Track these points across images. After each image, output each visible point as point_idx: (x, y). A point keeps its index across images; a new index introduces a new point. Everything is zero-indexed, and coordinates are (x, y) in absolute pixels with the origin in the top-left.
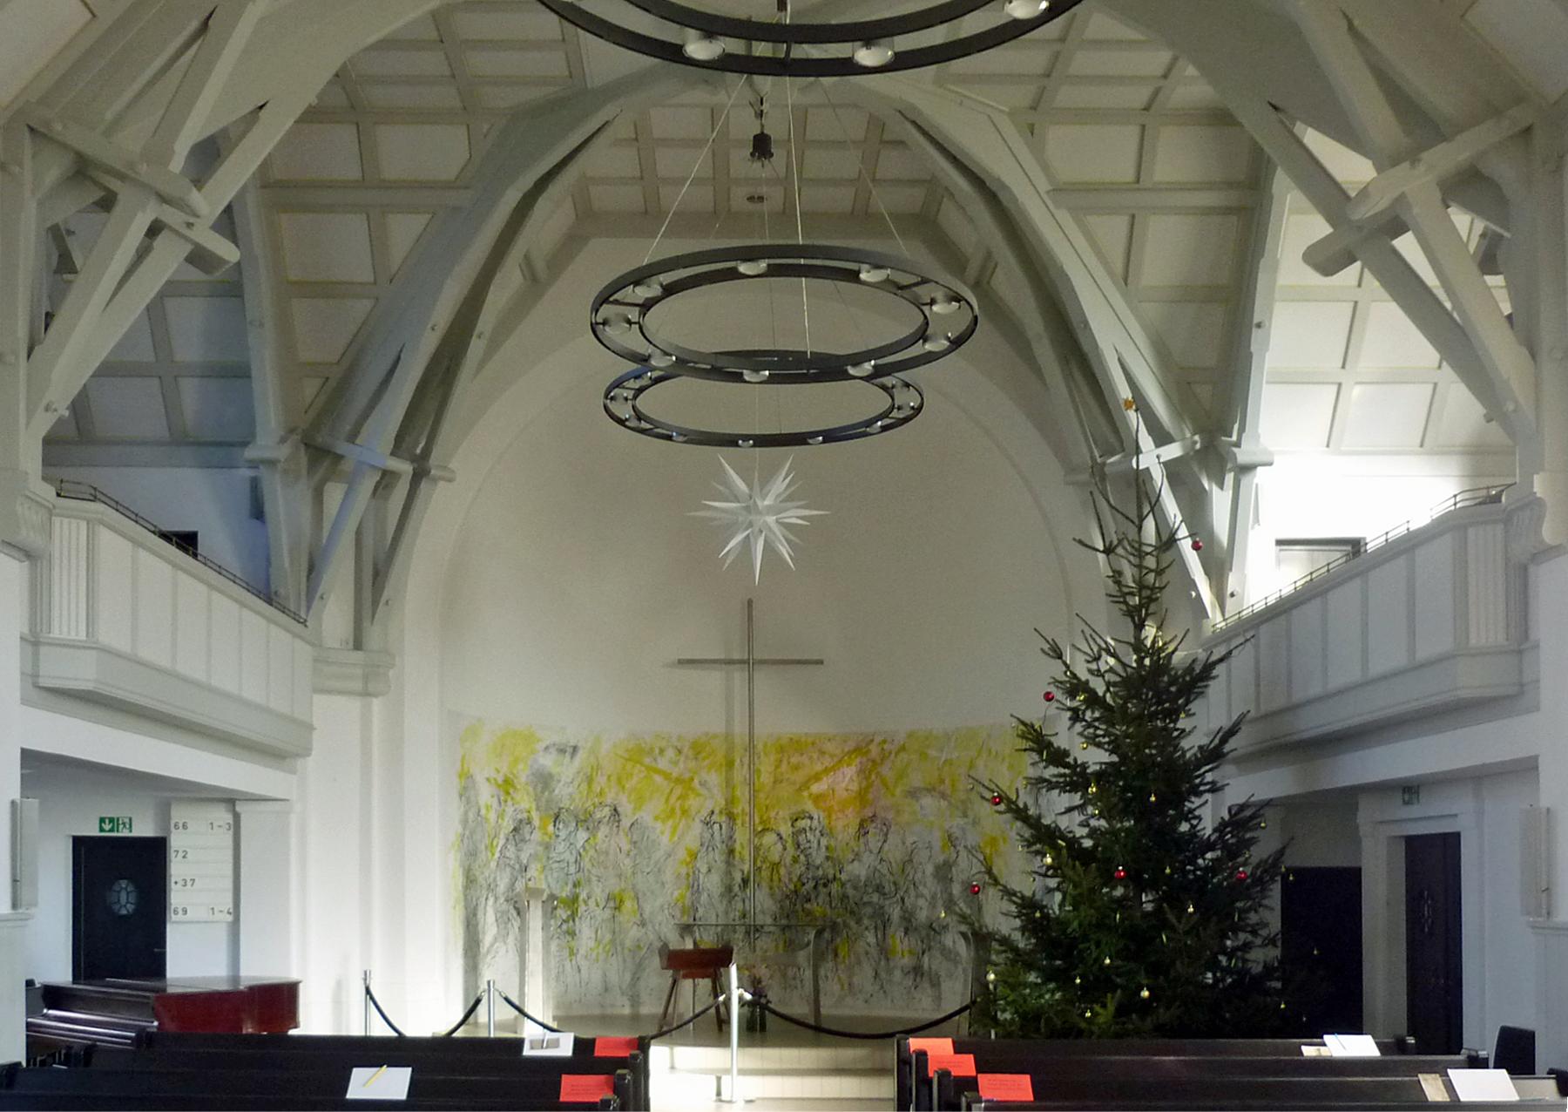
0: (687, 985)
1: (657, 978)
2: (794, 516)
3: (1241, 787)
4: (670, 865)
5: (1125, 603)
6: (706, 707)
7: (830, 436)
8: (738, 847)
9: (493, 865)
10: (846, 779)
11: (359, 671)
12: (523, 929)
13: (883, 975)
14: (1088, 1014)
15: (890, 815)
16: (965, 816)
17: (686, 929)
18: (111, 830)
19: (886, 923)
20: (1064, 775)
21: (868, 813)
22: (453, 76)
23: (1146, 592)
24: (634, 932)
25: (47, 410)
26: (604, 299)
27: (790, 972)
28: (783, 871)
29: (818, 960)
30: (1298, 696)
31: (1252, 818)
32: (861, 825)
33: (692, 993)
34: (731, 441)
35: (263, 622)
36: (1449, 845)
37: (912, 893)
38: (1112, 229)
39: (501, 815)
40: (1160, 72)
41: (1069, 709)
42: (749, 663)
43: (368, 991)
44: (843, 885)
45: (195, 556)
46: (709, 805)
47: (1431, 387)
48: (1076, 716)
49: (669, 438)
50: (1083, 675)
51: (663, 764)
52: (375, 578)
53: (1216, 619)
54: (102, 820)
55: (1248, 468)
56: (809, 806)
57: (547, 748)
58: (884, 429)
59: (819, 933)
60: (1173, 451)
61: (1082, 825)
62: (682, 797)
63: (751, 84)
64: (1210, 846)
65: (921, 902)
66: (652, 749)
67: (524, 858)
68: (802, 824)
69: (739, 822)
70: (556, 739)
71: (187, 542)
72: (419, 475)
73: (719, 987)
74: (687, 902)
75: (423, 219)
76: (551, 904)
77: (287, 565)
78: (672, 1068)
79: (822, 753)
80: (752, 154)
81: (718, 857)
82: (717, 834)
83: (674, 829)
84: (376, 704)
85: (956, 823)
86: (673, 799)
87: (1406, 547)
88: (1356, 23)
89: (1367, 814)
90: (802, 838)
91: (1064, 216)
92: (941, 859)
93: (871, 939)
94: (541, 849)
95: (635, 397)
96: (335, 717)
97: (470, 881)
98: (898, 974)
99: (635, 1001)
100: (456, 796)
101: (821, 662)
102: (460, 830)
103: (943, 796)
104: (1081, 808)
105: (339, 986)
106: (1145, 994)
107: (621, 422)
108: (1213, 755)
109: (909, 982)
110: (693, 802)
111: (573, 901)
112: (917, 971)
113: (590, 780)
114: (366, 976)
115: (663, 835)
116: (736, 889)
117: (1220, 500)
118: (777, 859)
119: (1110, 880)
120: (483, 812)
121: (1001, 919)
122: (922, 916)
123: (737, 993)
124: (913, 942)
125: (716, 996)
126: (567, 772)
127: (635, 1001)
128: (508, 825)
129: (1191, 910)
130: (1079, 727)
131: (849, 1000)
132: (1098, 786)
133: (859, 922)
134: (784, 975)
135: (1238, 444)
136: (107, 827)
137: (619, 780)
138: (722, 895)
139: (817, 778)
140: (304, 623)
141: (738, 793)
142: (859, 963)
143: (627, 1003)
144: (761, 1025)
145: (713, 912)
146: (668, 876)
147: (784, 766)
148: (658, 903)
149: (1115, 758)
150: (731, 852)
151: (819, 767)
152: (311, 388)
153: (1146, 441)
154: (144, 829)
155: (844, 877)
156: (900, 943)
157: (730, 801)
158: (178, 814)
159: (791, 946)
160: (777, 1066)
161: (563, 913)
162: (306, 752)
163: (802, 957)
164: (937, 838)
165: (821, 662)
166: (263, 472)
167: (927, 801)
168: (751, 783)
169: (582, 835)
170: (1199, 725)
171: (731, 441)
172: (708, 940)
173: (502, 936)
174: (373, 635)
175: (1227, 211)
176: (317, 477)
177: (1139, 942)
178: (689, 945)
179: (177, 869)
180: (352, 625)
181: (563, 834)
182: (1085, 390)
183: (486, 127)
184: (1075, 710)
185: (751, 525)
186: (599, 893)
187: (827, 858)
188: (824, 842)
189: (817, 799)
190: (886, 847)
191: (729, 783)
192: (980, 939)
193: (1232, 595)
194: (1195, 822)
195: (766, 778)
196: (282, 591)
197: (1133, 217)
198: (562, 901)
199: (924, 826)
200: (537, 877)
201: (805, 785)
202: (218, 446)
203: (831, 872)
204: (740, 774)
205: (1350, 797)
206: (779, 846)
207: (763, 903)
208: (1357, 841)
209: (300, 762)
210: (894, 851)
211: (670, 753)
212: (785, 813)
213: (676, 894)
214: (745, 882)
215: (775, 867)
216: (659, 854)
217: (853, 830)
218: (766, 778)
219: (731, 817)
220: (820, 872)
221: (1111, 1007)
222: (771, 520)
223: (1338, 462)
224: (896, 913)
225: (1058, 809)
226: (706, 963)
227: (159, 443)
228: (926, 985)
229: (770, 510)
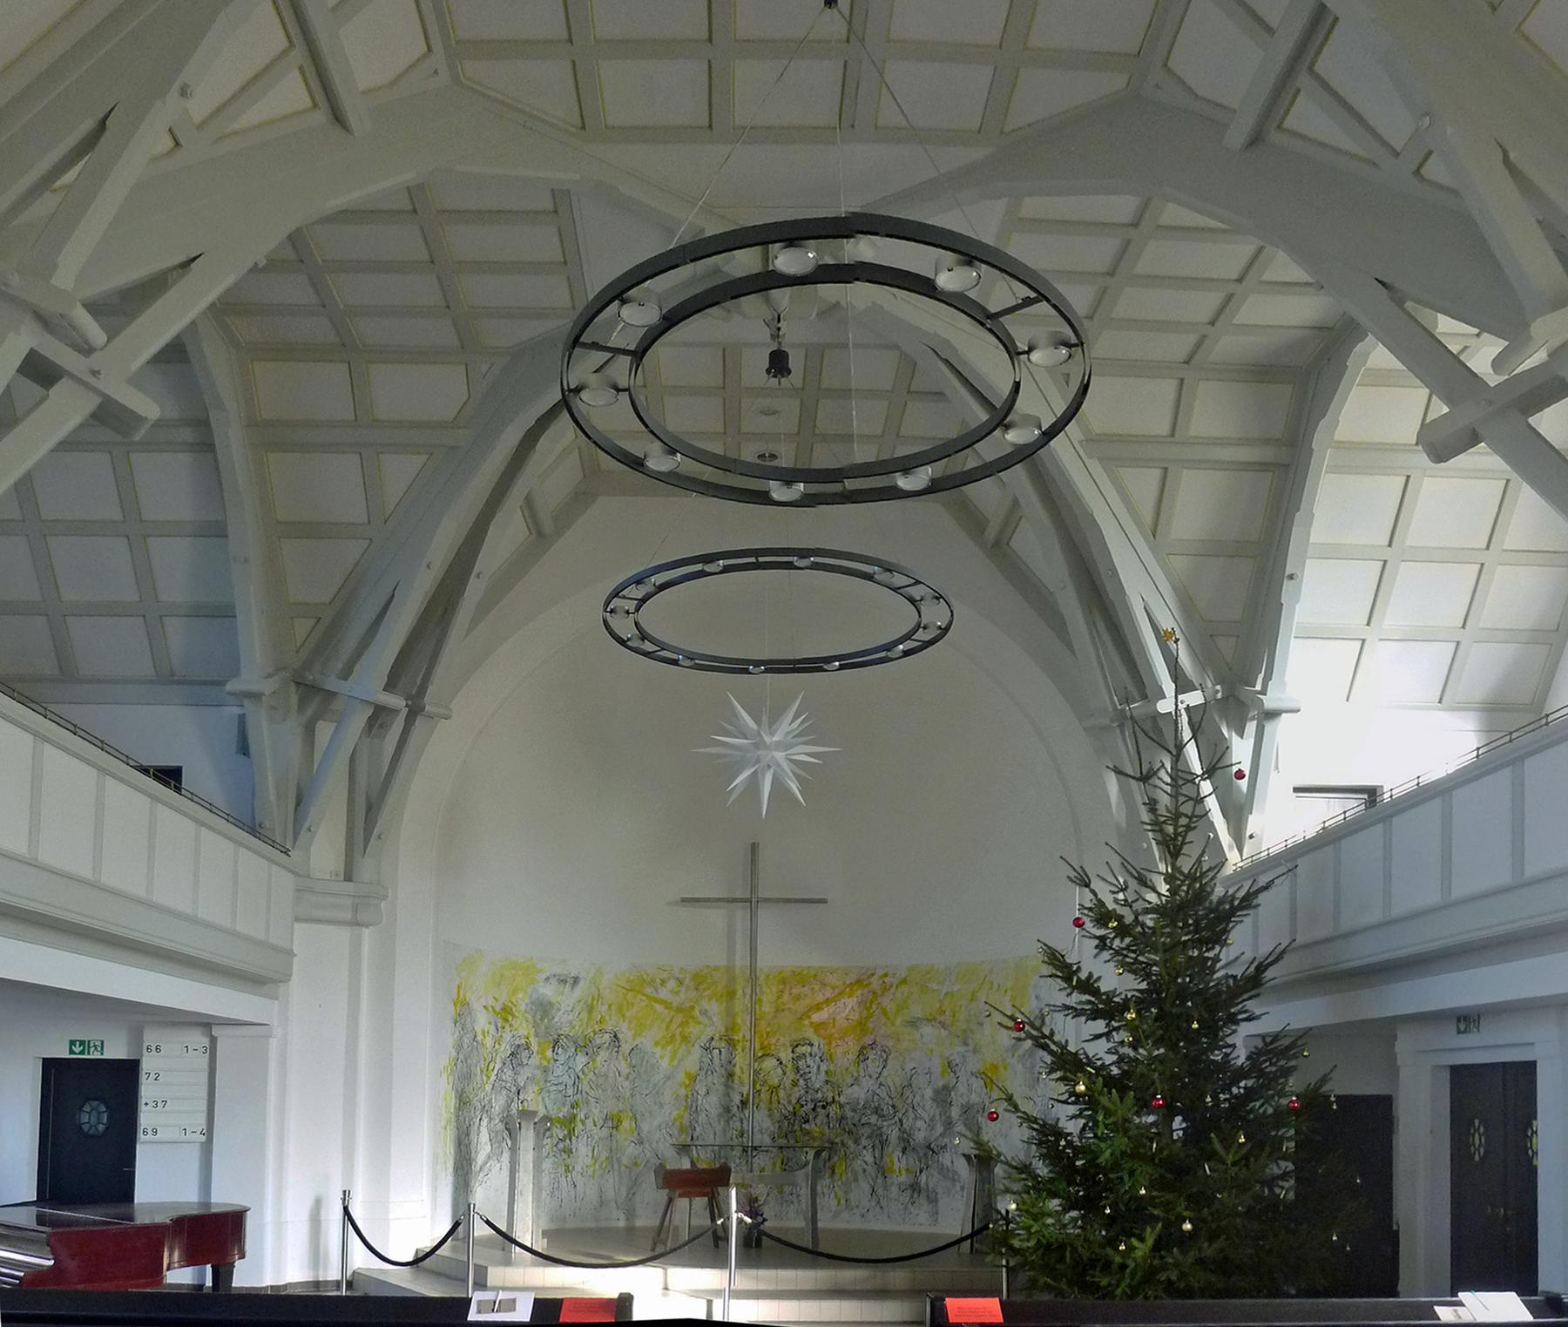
0: (682, 1203)
1: (652, 1195)
2: (803, 753)
3: (1269, 1017)
4: (668, 1089)
5: (1161, 831)
6: (707, 941)
7: (850, 662)
8: (737, 1070)
9: (488, 1088)
10: (847, 1008)
11: (349, 901)
12: (514, 1150)
13: (880, 1191)
14: (1122, 1247)
15: (890, 1044)
16: (966, 1044)
17: (683, 1149)
18: (82, 1053)
19: (884, 1143)
20: (1090, 1002)
21: (868, 1040)
22: (415, 211)
23: (1177, 828)
24: (631, 1150)
25: (576, 980)
26: (616, 594)
27: (787, 1189)
28: (782, 1094)
29: (817, 1173)
30: (1346, 925)
31: (1288, 1048)
32: (861, 1052)
33: (690, 1212)
34: (740, 667)
35: (230, 845)
36: (1519, 1080)
37: (911, 1115)
38: (1144, 483)
39: (498, 1041)
40: (1182, 356)
41: (1096, 937)
42: (752, 903)
43: (346, 1209)
44: (841, 1106)
45: (178, 790)
46: (709, 1032)
47: (1453, 645)
48: (1103, 944)
49: (675, 662)
50: (1111, 906)
51: (664, 994)
52: (368, 815)
53: (1234, 860)
54: (72, 1043)
55: (1273, 715)
56: (810, 1034)
57: (547, 979)
58: (907, 653)
59: (817, 1155)
60: (1194, 698)
61: (1109, 1052)
62: (683, 1024)
63: (767, 300)
64: (1241, 1074)
65: (920, 1124)
66: (653, 981)
67: (521, 1081)
68: (805, 1049)
69: (739, 1048)
70: (558, 970)
71: (170, 776)
72: (415, 711)
73: (716, 1208)
74: (686, 1122)
75: (419, 460)
76: (544, 1125)
77: (272, 798)
78: (666, 1289)
79: (824, 985)
80: (768, 371)
81: (717, 1080)
82: (716, 1060)
83: (675, 1052)
84: (366, 933)
85: (956, 1051)
86: (673, 1026)
87: (1423, 795)
88: (1512, 156)
89: (1405, 1045)
90: (801, 1063)
91: (1096, 467)
92: (940, 1084)
93: (869, 1158)
94: (538, 1072)
95: (637, 610)
96: (318, 949)
97: (463, 1102)
98: (895, 1190)
99: (630, 1214)
100: (450, 1024)
101: (824, 901)
102: (454, 1054)
103: (944, 1026)
104: (1107, 1035)
105: (318, 1204)
106: (1188, 1226)
107: (623, 642)
108: (1253, 982)
109: (906, 1197)
110: (693, 1030)
111: (572, 1119)
112: (915, 1188)
113: (590, 1009)
114: (346, 1195)
115: (663, 1060)
116: (735, 1110)
117: (1240, 751)
118: (776, 1082)
119: (1143, 1105)
120: (480, 1037)
121: (1011, 1140)
122: (920, 1136)
123: (736, 1215)
124: (911, 1160)
125: (713, 1220)
126: (567, 1002)
127: (630, 1214)
128: (505, 1049)
129: (1242, 1140)
130: (1106, 955)
131: (845, 1215)
132: (1138, 1012)
133: (856, 1142)
134: (781, 1192)
135: (1264, 692)
136: (77, 1049)
137: (620, 1009)
138: (720, 1115)
139: (818, 1007)
140: (286, 853)
141: (739, 1021)
142: (856, 1180)
143: (622, 1217)
144: (760, 1246)
145: (710, 1132)
146: (667, 1097)
147: (786, 997)
148: (656, 1123)
149: (1144, 985)
150: (731, 1075)
151: (820, 998)
152: (303, 627)
153: (1169, 687)
154: (116, 1050)
155: (842, 1099)
156: (898, 1162)
157: (731, 1028)
158: (150, 1037)
159: (788, 1166)
160: (772, 1287)
161: (560, 1132)
162: (286, 978)
163: (800, 1176)
164: (937, 1065)
165: (824, 901)
166: (249, 707)
167: (927, 1030)
168: (752, 1012)
169: (581, 1060)
170: (1240, 947)
171: (740, 667)
172: (705, 1159)
173: (495, 1155)
174: (366, 868)
175: (1262, 466)
176: (309, 712)
177: (1175, 1173)
178: (686, 1165)
179: (147, 1091)
180: (343, 857)
181: (562, 1059)
182: (1106, 637)
183: (484, 368)
184: (1102, 939)
185: (758, 761)
186: (597, 1113)
187: (827, 1082)
188: (823, 1067)
189: (818, 1027)
190: (885, 1072)
191: (730, 1013)
192: (983, 1160)
193: (1251, 837)
194: (1228, 1050)
195: (767, 1008)
196: (267, 824)
197: (1166, 469)
198: (559, 1121)
199: (922, 1052)
200: (533, 1100)
201: (806, 1015)
202: (201, 685)
203: (830, 1095)
204: (741, 1003)
205: (1386, 1030)
206: (779, 1071)
207: (762, 1124)
208: (1393, 1072)
209: (282, 988)
210: (893, 1077)
211: (672, 984)
212: (785, 1040)
213: (675, 1114)
214: (744, 1103)
215: (774, 1090)
216: (658, 1077)
217: (852, 1056)
218: (767, 1008)
219: (731, 1043)
220: (820, 1095)
221: (1150, 1241)
222: (780, 755)
223: (1354, 717)
224: (894, 1134)
225: (1078, 1034)
226: (705, 1182)
227: (152, 682)
228: (923, 1200)
229: (780, 746)
